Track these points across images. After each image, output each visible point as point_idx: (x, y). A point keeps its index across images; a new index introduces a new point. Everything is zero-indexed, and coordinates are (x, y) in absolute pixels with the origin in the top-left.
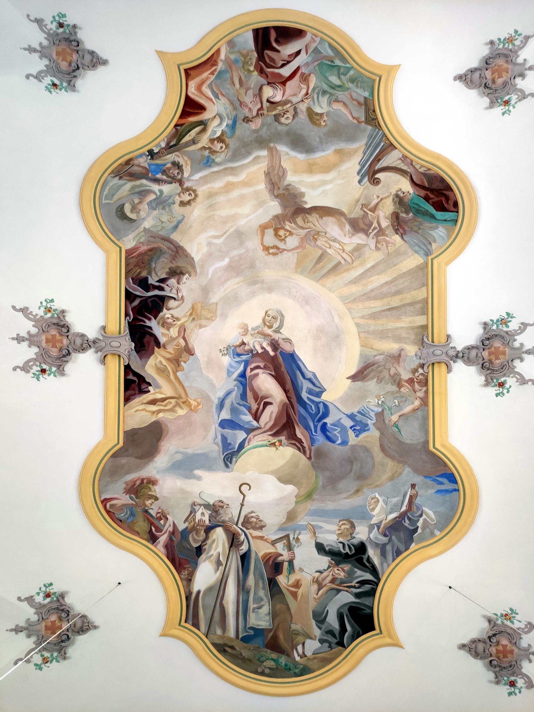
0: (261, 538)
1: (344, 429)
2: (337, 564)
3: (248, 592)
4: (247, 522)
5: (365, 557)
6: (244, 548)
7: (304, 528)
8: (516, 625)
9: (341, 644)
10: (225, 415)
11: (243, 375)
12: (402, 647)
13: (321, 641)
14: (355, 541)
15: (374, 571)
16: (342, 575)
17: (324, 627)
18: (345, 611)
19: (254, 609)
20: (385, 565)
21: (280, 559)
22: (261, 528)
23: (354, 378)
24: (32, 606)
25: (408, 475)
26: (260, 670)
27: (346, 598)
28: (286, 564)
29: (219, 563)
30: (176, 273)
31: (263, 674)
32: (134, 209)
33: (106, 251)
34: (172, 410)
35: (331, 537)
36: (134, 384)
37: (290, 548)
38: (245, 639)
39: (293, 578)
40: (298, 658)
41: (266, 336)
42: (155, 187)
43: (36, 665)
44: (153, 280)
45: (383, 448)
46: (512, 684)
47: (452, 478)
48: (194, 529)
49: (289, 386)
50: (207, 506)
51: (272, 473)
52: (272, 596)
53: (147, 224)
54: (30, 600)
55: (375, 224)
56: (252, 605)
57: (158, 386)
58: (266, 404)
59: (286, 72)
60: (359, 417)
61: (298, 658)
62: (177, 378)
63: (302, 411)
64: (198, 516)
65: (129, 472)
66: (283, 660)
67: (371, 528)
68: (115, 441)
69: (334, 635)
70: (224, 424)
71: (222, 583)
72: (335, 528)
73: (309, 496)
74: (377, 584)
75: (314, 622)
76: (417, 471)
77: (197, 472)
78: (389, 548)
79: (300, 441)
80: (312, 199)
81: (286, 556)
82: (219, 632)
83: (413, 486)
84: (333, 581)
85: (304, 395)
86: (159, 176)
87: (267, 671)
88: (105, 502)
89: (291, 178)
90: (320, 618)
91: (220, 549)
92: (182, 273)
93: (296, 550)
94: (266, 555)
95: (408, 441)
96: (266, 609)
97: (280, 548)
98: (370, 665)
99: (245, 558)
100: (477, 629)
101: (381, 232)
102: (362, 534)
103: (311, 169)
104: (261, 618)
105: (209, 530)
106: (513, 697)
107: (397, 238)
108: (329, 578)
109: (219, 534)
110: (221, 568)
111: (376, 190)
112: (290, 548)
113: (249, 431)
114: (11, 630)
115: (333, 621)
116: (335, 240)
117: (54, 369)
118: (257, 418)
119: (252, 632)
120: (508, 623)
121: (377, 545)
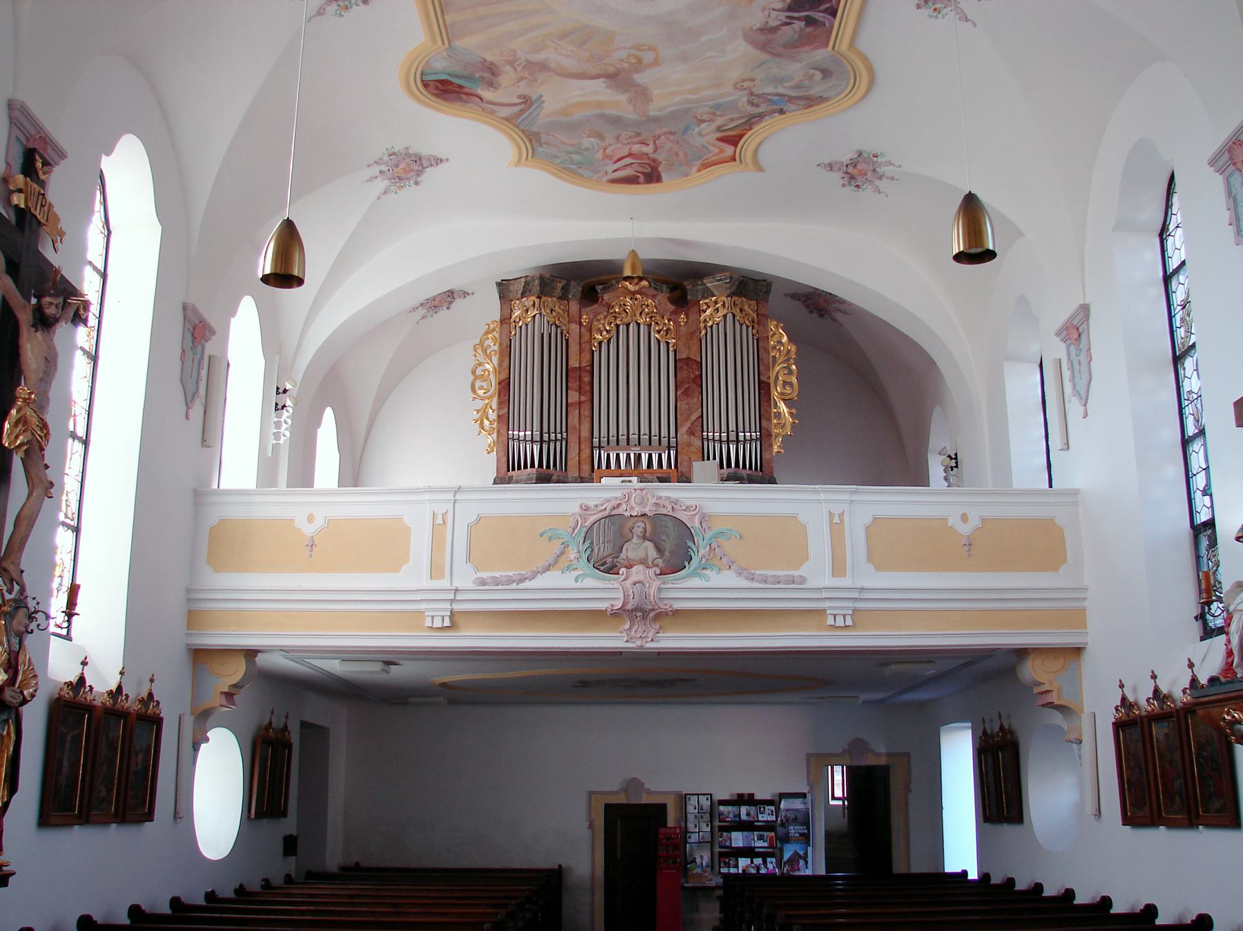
7: (838, 799)
30: (767, 30)
32: (811, 77)
42: (781, 90)
44: (799, 25)
53: (798, 65)
55: (519, 69)
59: (628, 161)
80: (600, 84)
86: (775, 98)
89: (623, 98)
92: (761, 30)
95: (718, 915)
101: (511, 63)
103: (600, 104)
107: (490, 58)
111: (523, 89)
116: (567, 56)
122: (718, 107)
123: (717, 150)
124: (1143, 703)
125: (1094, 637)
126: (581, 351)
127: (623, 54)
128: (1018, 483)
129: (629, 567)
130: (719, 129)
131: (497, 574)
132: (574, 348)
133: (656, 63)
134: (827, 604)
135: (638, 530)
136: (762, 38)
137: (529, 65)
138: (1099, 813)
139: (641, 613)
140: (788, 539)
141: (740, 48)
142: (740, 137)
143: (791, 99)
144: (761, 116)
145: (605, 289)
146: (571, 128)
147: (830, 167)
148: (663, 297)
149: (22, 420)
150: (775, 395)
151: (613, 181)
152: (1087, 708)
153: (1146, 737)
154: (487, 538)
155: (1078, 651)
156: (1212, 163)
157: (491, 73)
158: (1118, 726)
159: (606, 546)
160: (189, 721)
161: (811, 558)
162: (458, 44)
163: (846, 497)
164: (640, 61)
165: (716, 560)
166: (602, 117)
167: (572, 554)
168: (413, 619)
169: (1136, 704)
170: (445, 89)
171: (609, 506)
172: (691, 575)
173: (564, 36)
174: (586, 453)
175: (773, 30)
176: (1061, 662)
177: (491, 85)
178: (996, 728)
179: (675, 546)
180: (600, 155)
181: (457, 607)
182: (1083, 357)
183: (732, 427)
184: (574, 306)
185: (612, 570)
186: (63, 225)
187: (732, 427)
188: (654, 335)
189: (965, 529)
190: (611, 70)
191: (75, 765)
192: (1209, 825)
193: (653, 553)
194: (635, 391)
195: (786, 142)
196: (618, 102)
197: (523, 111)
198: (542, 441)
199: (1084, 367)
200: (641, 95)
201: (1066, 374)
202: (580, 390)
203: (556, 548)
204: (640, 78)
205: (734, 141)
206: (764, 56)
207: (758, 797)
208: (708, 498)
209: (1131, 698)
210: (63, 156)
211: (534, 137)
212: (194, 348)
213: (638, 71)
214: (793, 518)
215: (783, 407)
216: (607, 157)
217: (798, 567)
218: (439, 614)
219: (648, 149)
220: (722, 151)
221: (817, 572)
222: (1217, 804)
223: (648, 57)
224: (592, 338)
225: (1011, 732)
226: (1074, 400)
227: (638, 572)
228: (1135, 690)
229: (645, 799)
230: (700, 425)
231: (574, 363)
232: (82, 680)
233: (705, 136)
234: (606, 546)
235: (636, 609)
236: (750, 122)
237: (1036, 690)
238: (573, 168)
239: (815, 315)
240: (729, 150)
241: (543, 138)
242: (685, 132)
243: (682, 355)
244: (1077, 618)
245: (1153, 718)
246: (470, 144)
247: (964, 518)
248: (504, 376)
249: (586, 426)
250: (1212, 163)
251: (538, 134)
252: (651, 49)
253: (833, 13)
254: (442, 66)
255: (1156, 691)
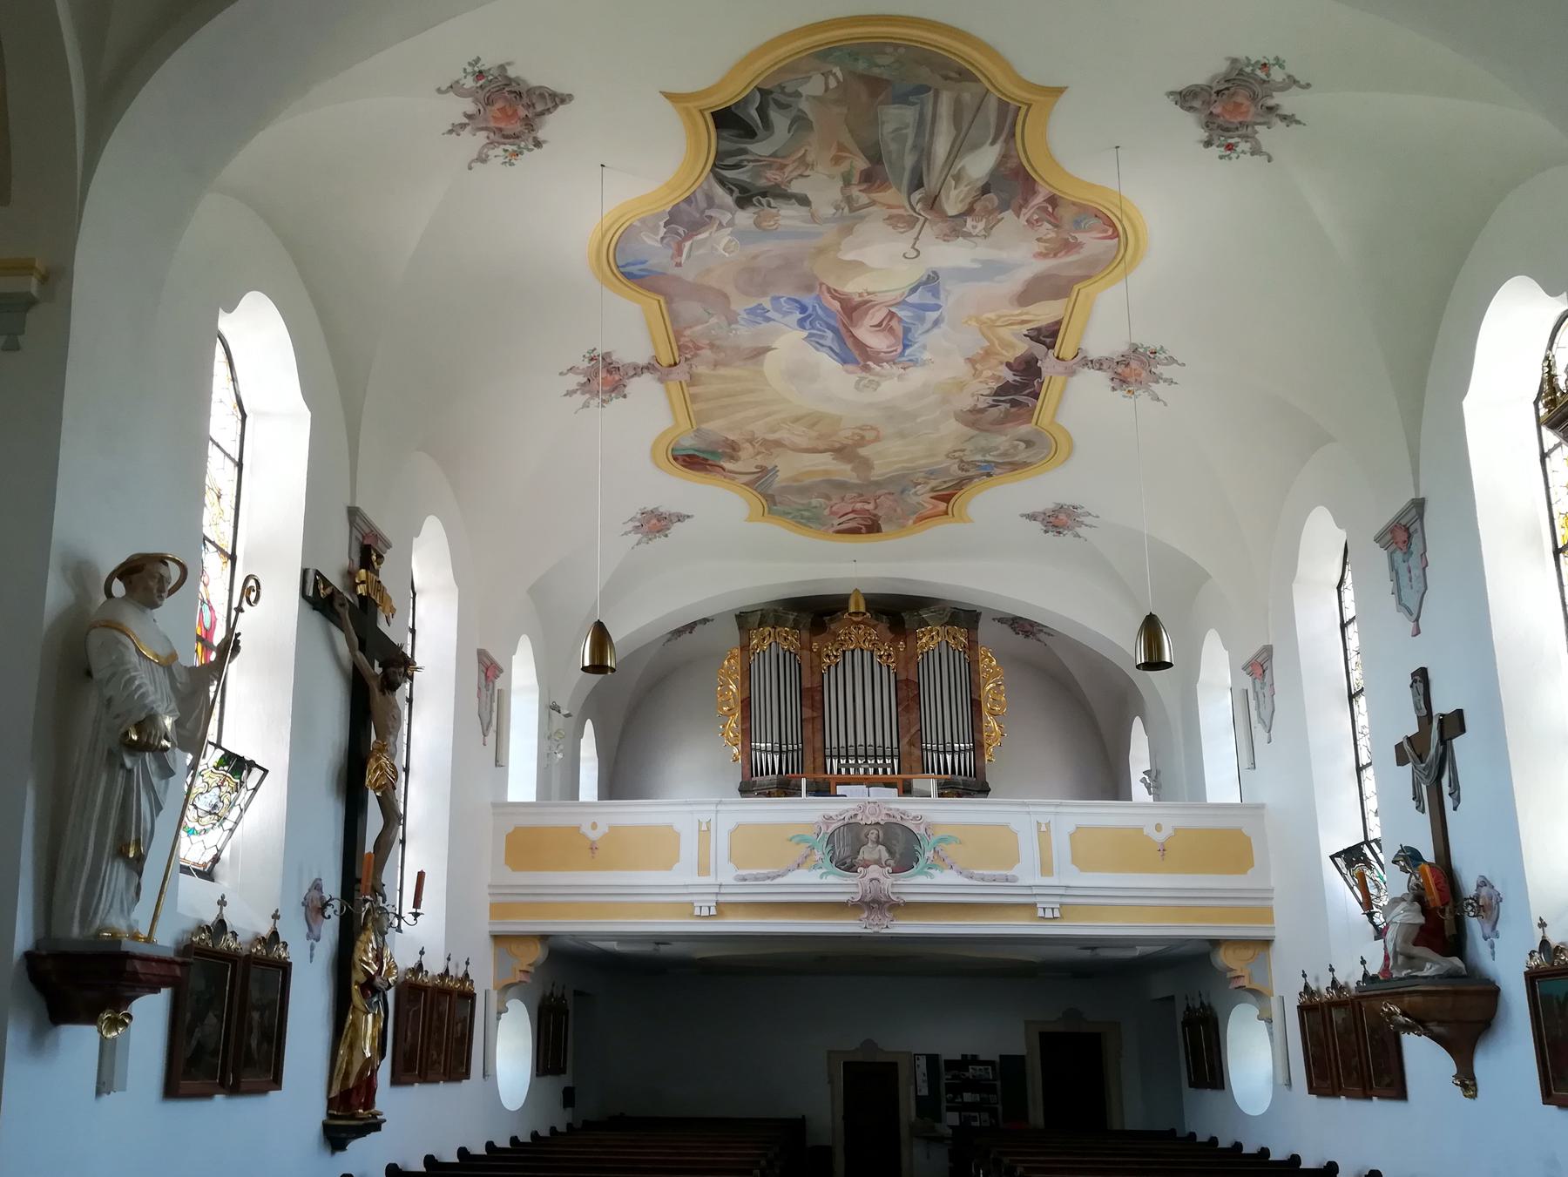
0: (890, 207)
1: (777, 310)
2: (777, 185)
3: (914, 147)
4: (911, 222)
5: (737, 193)
6: (917, 196)
7: (827, 220)
8: (499, 151)
9: (764, 93)
10: (933, 315)
11: (906, 346)
12: (669, 96)
13: (798, 95)
14: (752, 210)
15: (722, 182)
16: (769, 174)
17: (794, 113)
18: (761, 132)
19: (907, 126)
20: (705, 187)
21: (864, 186)
22: (890, 217)
23: (768, 349)
24: (1257, 142)
25: (689, 273)
26: (901, 50)
27: (759, 148)
28: (855, 180)
29: (958, 178)
30: (975, 411)
31: (897, 46)
33: (1052, 422)
34: (1000, 317)
35: (788, 215)
36: (1048, 336)
37: (849, 200)
38: (922, 89)
39: (845, 166)
40: (837, 70)
41: (877, 374)
42: (988, 458)
43: (1282, 66)
45: (725, 296)
46: (480, 75)
47: (629, 276)
48: (989, 212)
49: (849, 342)
50: (968, 235)
51: (872, 269)
52: (877, 143)
54: (1256, 151)
56: (910, 133)
57: (1015, 335)
58: (880, 325)
60: (759, 319)
61: (837, 70)
62: (988, 339)
63: (832, 322)
64: (981, 225)
65: (1070, 263)
66: (861, 66)
67: (731, 224)
68: (1084, 290)
69: (777, 103)
70: (937, 307)
71: (955, 153)
72: (782, 222)
73: (820, 251)
74: (714, 165)
75: (811, 117)
76: (677, 279)
77: (976, 266)
78: (703, 204)
79: (834, 298)
80: (827, 457)
81: (855, 191)
82: (967, 97)
83: (679, 265)
84: (782, 167)
85: (829, 334)
87: (889, 50)
88: (1116, 235)
89: (848, 467)
90: (800, 123)
91: (953, 193)
93: (839, 196)
94: (884, 190)
96: (888, 128)
97: (864, 199)
98: (718, 63)
99: (917, 183)
100: (553, 126)
101: (750, 442)
102: (745, 218)
103: (826, 472)
104: (896, 118)
105: (970, 211)
106: (472, 58)
107: (731, 437)
108: (787, 170)
109: (952, 209)
110: (954, 171)
111: (760, 460)
112: (849, 200)
113: (902, 303)
114: (1298, 122)
115: (779, 120)
117: (1248, 70)
118: (892, 315)
119: (912, 99)
120: (510, 148)
121: (721, 207)
122: (932, 473)
123: (929, 505)
124: (1324, 991)
125: (1281, 930)
126: (812, 673)
127: (848, 433)
128: (1212, 798)
129: (866, 866)
130: (933, 490)
131: (754, 872)
132: (806, 671)
133: (877, 439)
134: (1038, 899)
135: (872, 836)
136: (972, 417)
137: (765, 442)
138: (1289, 1083)
139: (874, 904)
140: (1002, 846)
141: (953, 426)
142: (952, 495)
143: (997, 465)
144: (971, 479)
145: (831, 621)
146: (804, 491)
147: (1032, 517)
148: (883, 626)
149: (380, 767)
150: (985, 712)
151: (838, 532)
152: (1276, 993)
153: (1327, 1021)
154: (745, 842)
155: (1267, 943)
156: (1377, 540)
157: (732, 450)
158: (1302, 1009)
159: (845, 848)
160: (494, 996)
161: (1029, 859)
162: (705, 426)
163: (1052, 809)
164: (863, 437)
165: (941, 862)
166: (829, 482)
167: (818, 855)
168: (687, 909)
169: (1318, 991)
170: (693, 461)
171: (847, 815)
172: (919, 873)
173: (797, 420)
174: (820, 760)
175: (982, 411)
176: (1250, 953)
177: (733, 458)
178: (1198, 1005)
179: (904, 848)
180: (826, 512)
181: (722, 899)
182: (1267, 690)
183: (948, 739)
184: (806, 635)
185: (851, 868)
186: (395, 603)
187: (948, 739)
188: (877, 660)
189: (1160, 837)
190: (837, 445)
191: (415, 1034)
192: (1380, 1097)
193: (885, 855)
194: (860, 704)
195: (998, 504)
196: (844, 471)
197: (759, 479)
198: (781, 752)
199: (1268, 699)
200: (866, 464)
201: (1253, 703)
202: (813, 707)
203: (803, 849)
204: (863, 451)
205: (946, 499)
206: (973, 432)
207: (982, 1058)
208: (930, 811)
209: (1313, 987)
210: (388, 546)
211: (771, 496)
212: (487, 686)
213: (862, 446)
214: (1006, 826)
215: (993, 724)
216: (832, 513)
217: (1011, 867)
218: (706, 904)
219: (870, 507)
220: (935, 507)
221: (1027, 874)
222: (1387, 1080)
223: (869, 435)
224: (821, 662)
225: (1210, 1007)
226: (1260, 726)
227: (874, 871)
228: (1317, 979)
229: (880, 1058)
230: (920, 736)
231: (806, 684)
232: (420, 965)
233: (921, 497)
234: (845, 848)
235: (874, 901)
236: (961, 484)
237: (1229, 975)
238: (806, 519)
239: (1021, 637)
240: (943, 506)
241: (778, 499)
242: (902, 492)
243: (902, 677)
244: (1266, 915)
245: (1332, 1004)
246: (716, 504)
247: (1158, 828)
248: (746, 695)
249: (819, 737)
250: (1377, 540)
251: (772, 496)
252: (872, 428)
253: (1036, 396)
254: (689, 443)
255: (1334, 981)
